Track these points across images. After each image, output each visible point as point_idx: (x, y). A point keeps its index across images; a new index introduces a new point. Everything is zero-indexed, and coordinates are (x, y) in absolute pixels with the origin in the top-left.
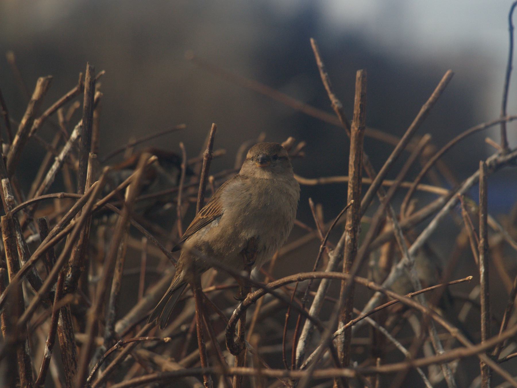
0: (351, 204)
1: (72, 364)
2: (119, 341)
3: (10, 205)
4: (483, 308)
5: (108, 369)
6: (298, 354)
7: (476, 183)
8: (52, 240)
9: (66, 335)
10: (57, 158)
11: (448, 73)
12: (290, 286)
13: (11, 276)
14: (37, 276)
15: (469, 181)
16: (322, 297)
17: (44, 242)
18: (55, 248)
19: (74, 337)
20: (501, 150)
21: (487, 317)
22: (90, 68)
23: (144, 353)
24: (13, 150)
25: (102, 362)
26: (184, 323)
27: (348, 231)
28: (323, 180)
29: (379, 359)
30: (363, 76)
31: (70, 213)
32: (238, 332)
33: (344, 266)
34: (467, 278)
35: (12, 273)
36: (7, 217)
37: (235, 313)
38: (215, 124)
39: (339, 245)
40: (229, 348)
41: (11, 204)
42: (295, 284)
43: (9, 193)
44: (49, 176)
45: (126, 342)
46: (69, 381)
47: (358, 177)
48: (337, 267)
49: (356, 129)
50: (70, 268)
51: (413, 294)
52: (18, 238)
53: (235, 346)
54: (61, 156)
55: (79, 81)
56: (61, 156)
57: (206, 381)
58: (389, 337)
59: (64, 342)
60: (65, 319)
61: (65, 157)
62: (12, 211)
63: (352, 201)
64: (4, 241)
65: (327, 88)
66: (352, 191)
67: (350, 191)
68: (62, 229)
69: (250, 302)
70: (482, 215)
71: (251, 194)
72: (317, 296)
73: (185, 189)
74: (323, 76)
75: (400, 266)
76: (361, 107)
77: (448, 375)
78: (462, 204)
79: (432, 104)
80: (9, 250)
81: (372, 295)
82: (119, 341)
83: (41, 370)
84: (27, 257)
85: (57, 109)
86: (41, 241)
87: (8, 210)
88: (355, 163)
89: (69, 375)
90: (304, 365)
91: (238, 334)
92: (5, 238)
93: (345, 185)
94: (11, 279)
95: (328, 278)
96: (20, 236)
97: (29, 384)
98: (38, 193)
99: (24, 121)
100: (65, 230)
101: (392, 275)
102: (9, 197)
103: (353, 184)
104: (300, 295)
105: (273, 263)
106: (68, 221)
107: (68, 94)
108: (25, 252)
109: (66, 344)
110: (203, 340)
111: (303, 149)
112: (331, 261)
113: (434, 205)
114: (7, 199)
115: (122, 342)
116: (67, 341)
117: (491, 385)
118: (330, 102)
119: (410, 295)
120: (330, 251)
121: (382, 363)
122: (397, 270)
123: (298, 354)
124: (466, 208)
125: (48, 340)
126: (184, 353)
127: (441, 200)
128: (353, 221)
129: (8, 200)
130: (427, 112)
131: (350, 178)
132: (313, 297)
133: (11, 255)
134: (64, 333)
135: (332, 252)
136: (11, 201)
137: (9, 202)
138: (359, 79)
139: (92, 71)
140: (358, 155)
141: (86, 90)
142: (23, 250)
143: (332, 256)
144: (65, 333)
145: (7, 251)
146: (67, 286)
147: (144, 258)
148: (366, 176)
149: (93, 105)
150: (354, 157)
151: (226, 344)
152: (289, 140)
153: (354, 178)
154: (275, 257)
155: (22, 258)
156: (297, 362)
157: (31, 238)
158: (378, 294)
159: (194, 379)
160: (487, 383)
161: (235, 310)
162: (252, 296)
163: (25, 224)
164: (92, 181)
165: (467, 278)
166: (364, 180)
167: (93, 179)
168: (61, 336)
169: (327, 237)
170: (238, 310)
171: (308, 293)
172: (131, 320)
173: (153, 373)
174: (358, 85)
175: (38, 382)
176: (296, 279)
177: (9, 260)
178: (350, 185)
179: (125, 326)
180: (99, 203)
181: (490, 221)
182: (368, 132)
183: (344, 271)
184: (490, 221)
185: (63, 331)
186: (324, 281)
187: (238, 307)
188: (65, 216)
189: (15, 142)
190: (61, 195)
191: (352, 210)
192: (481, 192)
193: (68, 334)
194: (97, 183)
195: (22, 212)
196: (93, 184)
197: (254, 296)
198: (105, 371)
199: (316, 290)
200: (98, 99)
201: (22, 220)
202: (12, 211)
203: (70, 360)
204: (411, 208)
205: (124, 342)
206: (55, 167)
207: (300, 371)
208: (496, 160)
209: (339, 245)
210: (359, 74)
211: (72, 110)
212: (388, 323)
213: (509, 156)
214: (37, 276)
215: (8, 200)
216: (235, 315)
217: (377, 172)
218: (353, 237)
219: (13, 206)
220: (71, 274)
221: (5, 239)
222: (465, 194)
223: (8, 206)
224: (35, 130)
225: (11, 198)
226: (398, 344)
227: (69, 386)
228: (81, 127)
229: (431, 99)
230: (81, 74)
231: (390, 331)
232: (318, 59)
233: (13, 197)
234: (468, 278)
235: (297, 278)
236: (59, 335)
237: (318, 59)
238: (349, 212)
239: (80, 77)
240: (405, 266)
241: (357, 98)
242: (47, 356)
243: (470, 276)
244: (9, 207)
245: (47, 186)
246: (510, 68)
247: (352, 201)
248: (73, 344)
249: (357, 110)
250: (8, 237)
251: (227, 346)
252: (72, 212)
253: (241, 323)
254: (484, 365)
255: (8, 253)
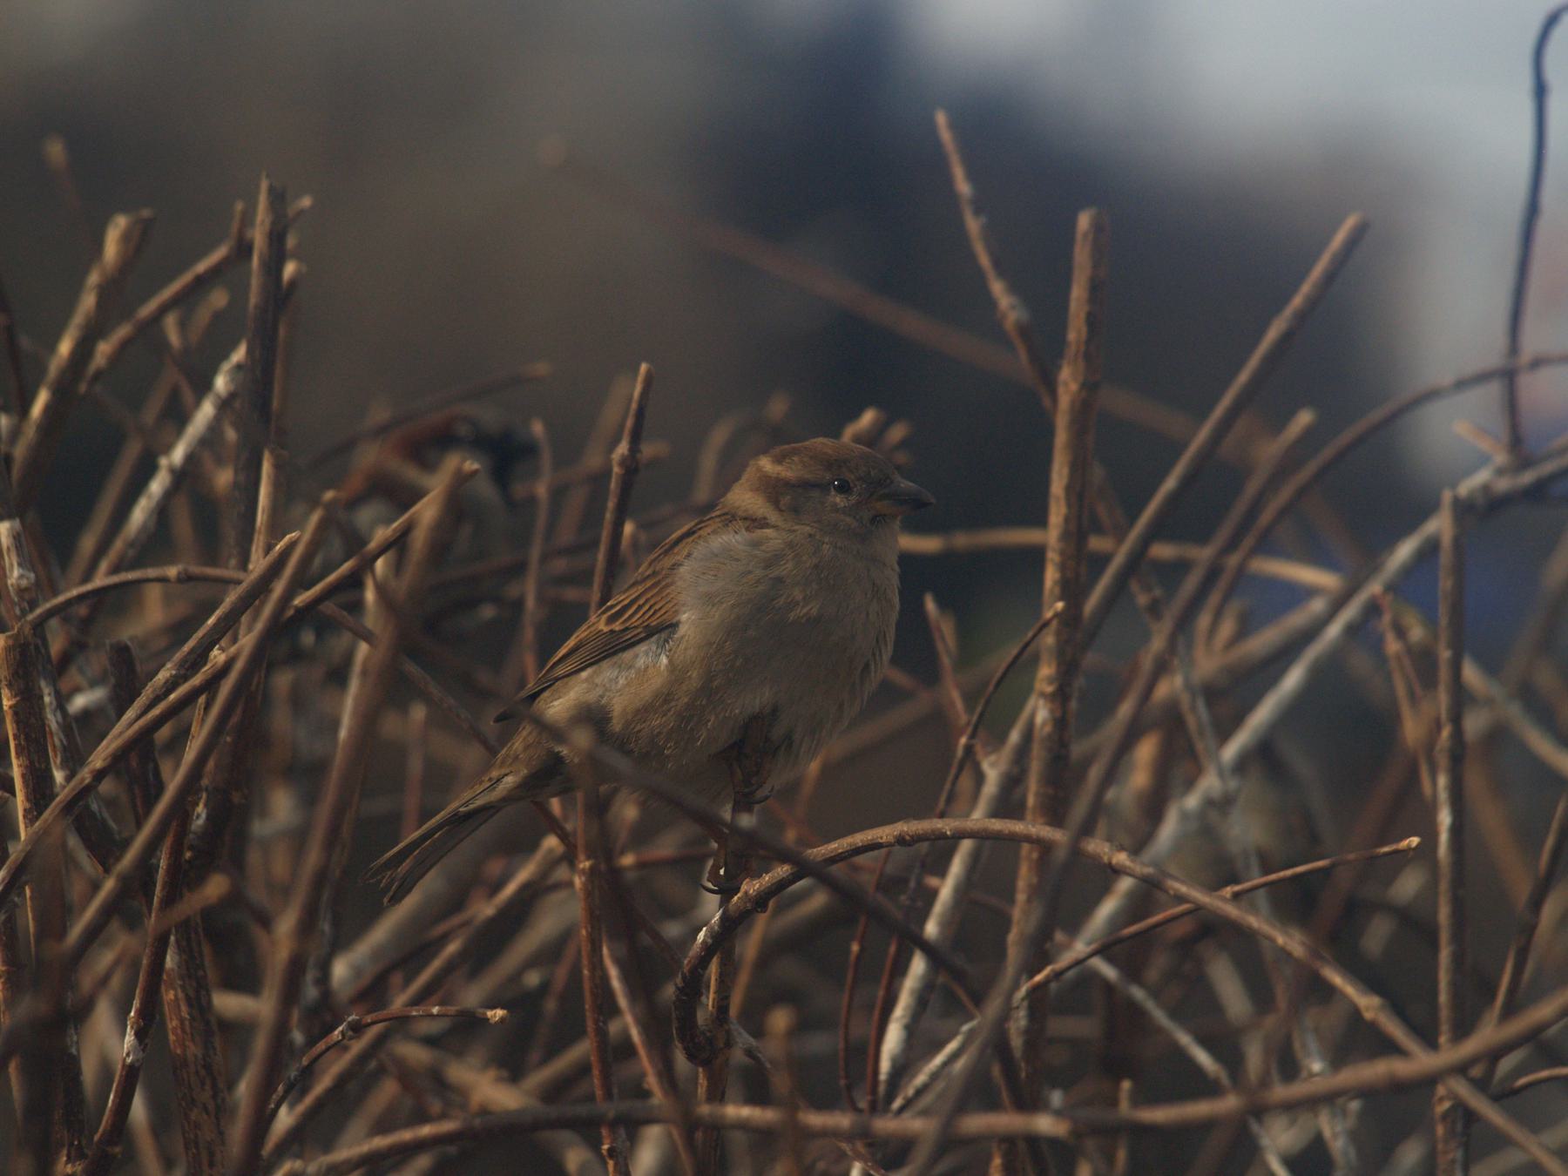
0: (1056, 615)
1: (203, 1084)
2: (350, 1019)
3: (21, 598)
4: (1444, 936)
5: (309, 1100)
6: (885, 1065)
7: (1430, 550)
8: (156, 711)
9: (187, 995)
10: (163, 462)
11: (1350, 222)
12: (860, 860)
13: (24, 817)
14: (102, 818)
15: (1405, 551)
16: (962, 892)
17: (130, 714)
18: (164, 733)
19: (210, 1002)
20: (1501, 458)
21: (1458, 959)
22: (271, 190)
23: (414, 1053)
24: (30, 432)
25: (295, 1079)
26: (533, 962)
27: (1043, 695)
28: (962, 540)
29: (1126, 1085)
30: (1097, 228)
31: (208, 628)
32: (712, 996)
33: (1031, 801)
34: (1404, 844)
35: (28, 805)
36: (16, 637)
37: (702, 938)
38: (648, 365)
39: (1015, 736)
40: (682, 1043)
41: (27, 596)
42: (884, 851)
43: (20, 565)
44: (140, 514)
45: (369, 1021)
46: (192, 1136)
47: (1077, 533)
48: (1007, 805)
49: (1074, 387)
50: (204, 795)
51: (1237, 888)
52: (47, 699)
53: (701, 1038)
54: (178, 454)
55: (235, 227)
56: (178, 454)
57: (608, 1141)
58: (1160, 1016)
59: (181, 1016)
60: (187, 951)
61: (190, 458)
62: (30, 617)
63: (1060, 605)
64: (5, 708)
65: (984, 260)
66: (1057, 576)
67: (1051, 575)
68: (186, 678)
69: (749, 906)
70: (1445, 654)
71: (779, 580)
72: (946, 891)
73: (545, 558)
74: (973, 225)
75: (1192, 801)
76: (1092, 321)
77: (1335, 1136)
78: (1387, 619)
79: (1302, 317)
80: (20, 736)
81: (1104, 890)
82: (350, 1019)
83: (113, 1101)
84: (74, 761)
85: (164, 310)
86: (112, 713)
87: (16, 616)
88: (1069, 489)
89: (193, 1117)
90: (904, 1098)
91: (710, 1000)
92: (8, 700)
93: (1035, 556)
94: (25, 823)
95: (979, 836)
96: (53, 694)
97: (76, 1143)
98: (104, 566)
99: (65, 347)
100: (197, 680)
101: (1169, 829)
102: (21, 577)
103: (1062, 553)
104: (892, 885)
105: (807, 788)
106: (200, 656)
107: (201, 267)
108: (65, 742)
109: (187, 1023)
110: (601, 1018)
111: (904, 444)
112: (991, 787)
113: (1297, 620)
114: (14, 581)
115: (359, 1021)
116: (189, 1014)
117: (1466, 1168)
118: (991, 303)
119: (1228, 891)
120: (988, 754)
121: (1139, 1099)
122: (1185, 816)
123: (885, 1065)
124: (1401, 632)
125: (135, 1013)
126: (535, 1056)
127: (1318, 606)
128: (1059, 665)
129: (18, 586)
130: (1287, 338)
131: (1051, 536)
132: (933, 894)
133: (26, 751)
134: (179, 991)
135: (993, 758)
136: (26, 589)
137: (21, 591)
138: (1085, 235)
139: (278, 199)
140: (1078, 467)
141: (260, 258)
142: (62, 737)
143: (993, 771)
144: (183, 991)
145: (15, 739)
146: (191, 848)
147: (415, 766)
148: (1099, 529)
149: (279, 297)
150: (1065, 471)
151: (674, 1032)
152: (868, 418)
153: (1065, 536)
154: (814, 767)
155: (58, 761)
156: (882, 1089)
157: (79, 702)
158: (1125, 884)
159: (566, 1135)
160: (1453, 1161)
161: (704, 929)
162: (756, 888)
163: (66, 660)
164: (277, 528)
165: (1404, 844)
166: (1097, 543)
167: (277, 528)
168: (172, 997)
169: (981, 715)
170: (712, 928)
171: (920, 883)
172: (376, 954)
173: (443, 1116)
174: (1082, 256)
175: (102, 1135)
176: (891, 839)
177: (20, 766)
178: (1053, 556)
179: (357, 971)
180: (300, 600)
181: (1471, 674)
182: (1120, 402)
183: (1029, 816)
184: (1471, 674)
185: (180, 982)
186: (966, 845)
187: (713, 921)
188: (194, 637)
189: (37, 409)
190: (179, 573)
191: (1058, 634)
192: (1445, 583)
193: (192, 993)
194: (300, 536)
195: (54, 623)
196: (280, 541)
197: (762, 888)
198: (301, 1108)
199: (942, 873)
200: (293, 283)
201: (56, 645)
202: (30, 617)
203: (197, 1072)
204: (1227, 628)
205: (364, 1022)
206: (157, 486)
207: (890, 1115)
208: (1486, 488)
209: (1015, 736)
210: (1084, 221)
211: (203, 316)
212: (1153, 974)
213: (1528, 478)
214: (101, 815)
215: (18, 586)
216: (701, 943)
217: (1133, 518)
218: (1058, 714)
219: (33, 605)
220: (205, 811)
221: (10, 703)
222: (1398, 587)
223: (16, 604)
224: (98, 375)
225: (28, 579)
226: (1185, 1039)
227: (194, 1151)
228: (239, 367)
229: (1297, 301)
230: (239, 206)
231: (1155, 993)
232: (959, 173)
233: (32, 575)
234: (1408, 841)
235: (895, 837)
236: (167, 995)
237: (959, 173)
238: (1049, 639)
239: (237, 216)
240: (1209, 803)
241: (1078, 293)
242: (131, 1058)
243: (1411, 839)
244: (20, 606)
245: (131, 544)
246: (1533, 209)
247: (1060, 605)
248: (207, 1023)
249: (1076, 332)
250: (18, 698)
251: (675, 1036)
252: (215, 625)
253: (721, 968)
254: (1447, 1105)
255: (16, 746)
